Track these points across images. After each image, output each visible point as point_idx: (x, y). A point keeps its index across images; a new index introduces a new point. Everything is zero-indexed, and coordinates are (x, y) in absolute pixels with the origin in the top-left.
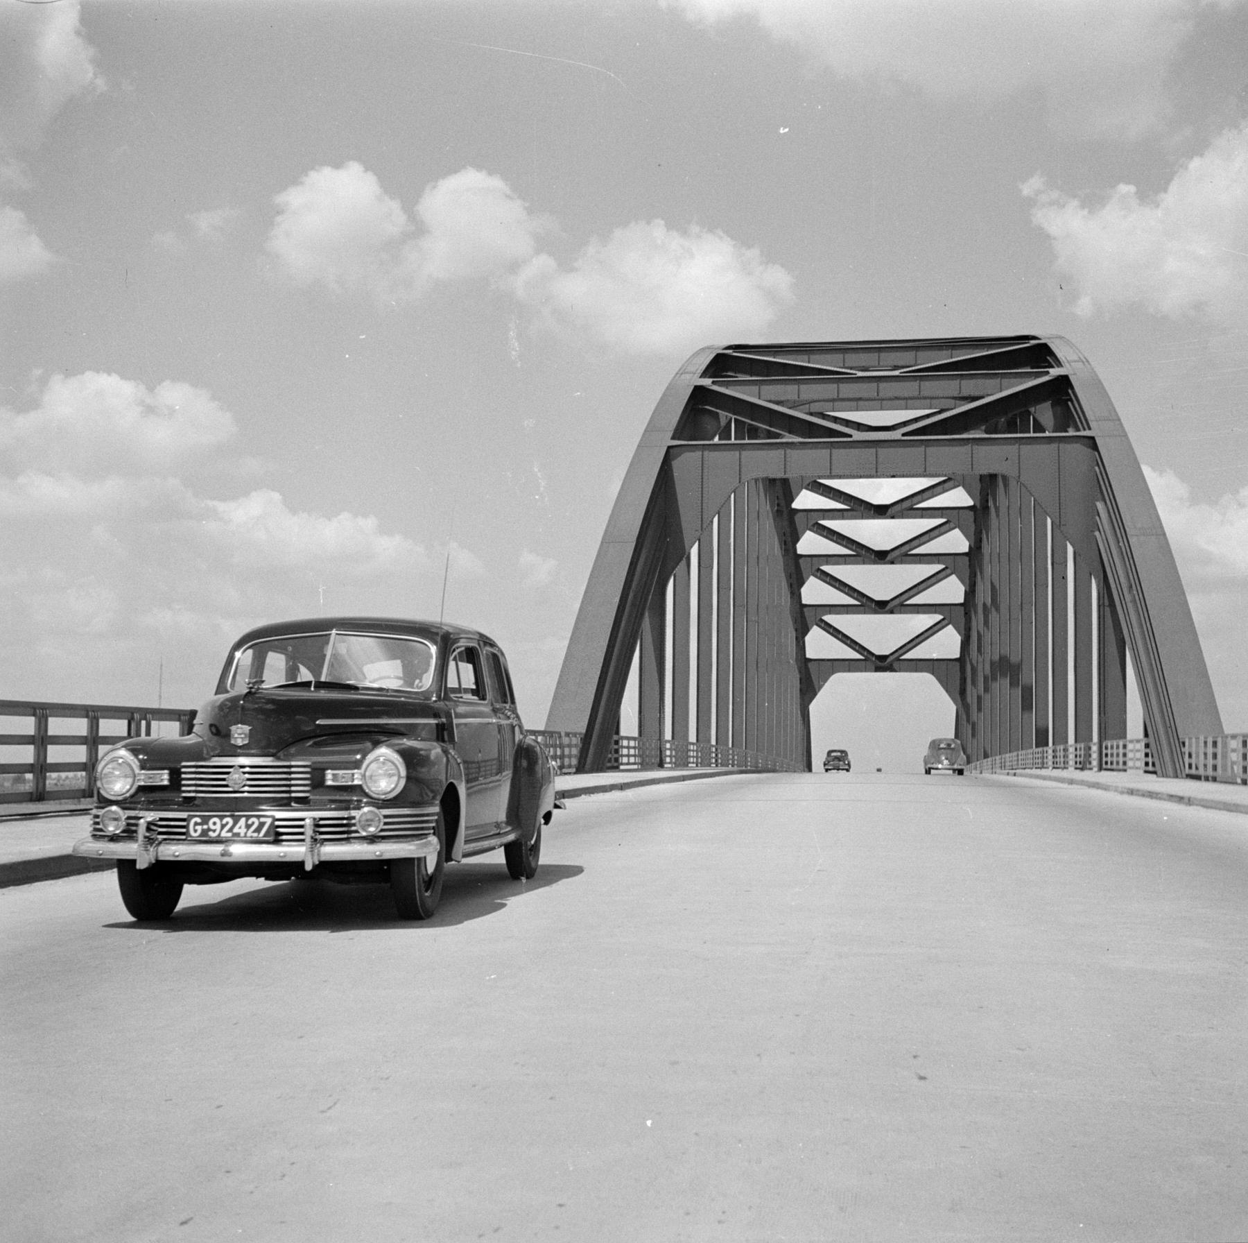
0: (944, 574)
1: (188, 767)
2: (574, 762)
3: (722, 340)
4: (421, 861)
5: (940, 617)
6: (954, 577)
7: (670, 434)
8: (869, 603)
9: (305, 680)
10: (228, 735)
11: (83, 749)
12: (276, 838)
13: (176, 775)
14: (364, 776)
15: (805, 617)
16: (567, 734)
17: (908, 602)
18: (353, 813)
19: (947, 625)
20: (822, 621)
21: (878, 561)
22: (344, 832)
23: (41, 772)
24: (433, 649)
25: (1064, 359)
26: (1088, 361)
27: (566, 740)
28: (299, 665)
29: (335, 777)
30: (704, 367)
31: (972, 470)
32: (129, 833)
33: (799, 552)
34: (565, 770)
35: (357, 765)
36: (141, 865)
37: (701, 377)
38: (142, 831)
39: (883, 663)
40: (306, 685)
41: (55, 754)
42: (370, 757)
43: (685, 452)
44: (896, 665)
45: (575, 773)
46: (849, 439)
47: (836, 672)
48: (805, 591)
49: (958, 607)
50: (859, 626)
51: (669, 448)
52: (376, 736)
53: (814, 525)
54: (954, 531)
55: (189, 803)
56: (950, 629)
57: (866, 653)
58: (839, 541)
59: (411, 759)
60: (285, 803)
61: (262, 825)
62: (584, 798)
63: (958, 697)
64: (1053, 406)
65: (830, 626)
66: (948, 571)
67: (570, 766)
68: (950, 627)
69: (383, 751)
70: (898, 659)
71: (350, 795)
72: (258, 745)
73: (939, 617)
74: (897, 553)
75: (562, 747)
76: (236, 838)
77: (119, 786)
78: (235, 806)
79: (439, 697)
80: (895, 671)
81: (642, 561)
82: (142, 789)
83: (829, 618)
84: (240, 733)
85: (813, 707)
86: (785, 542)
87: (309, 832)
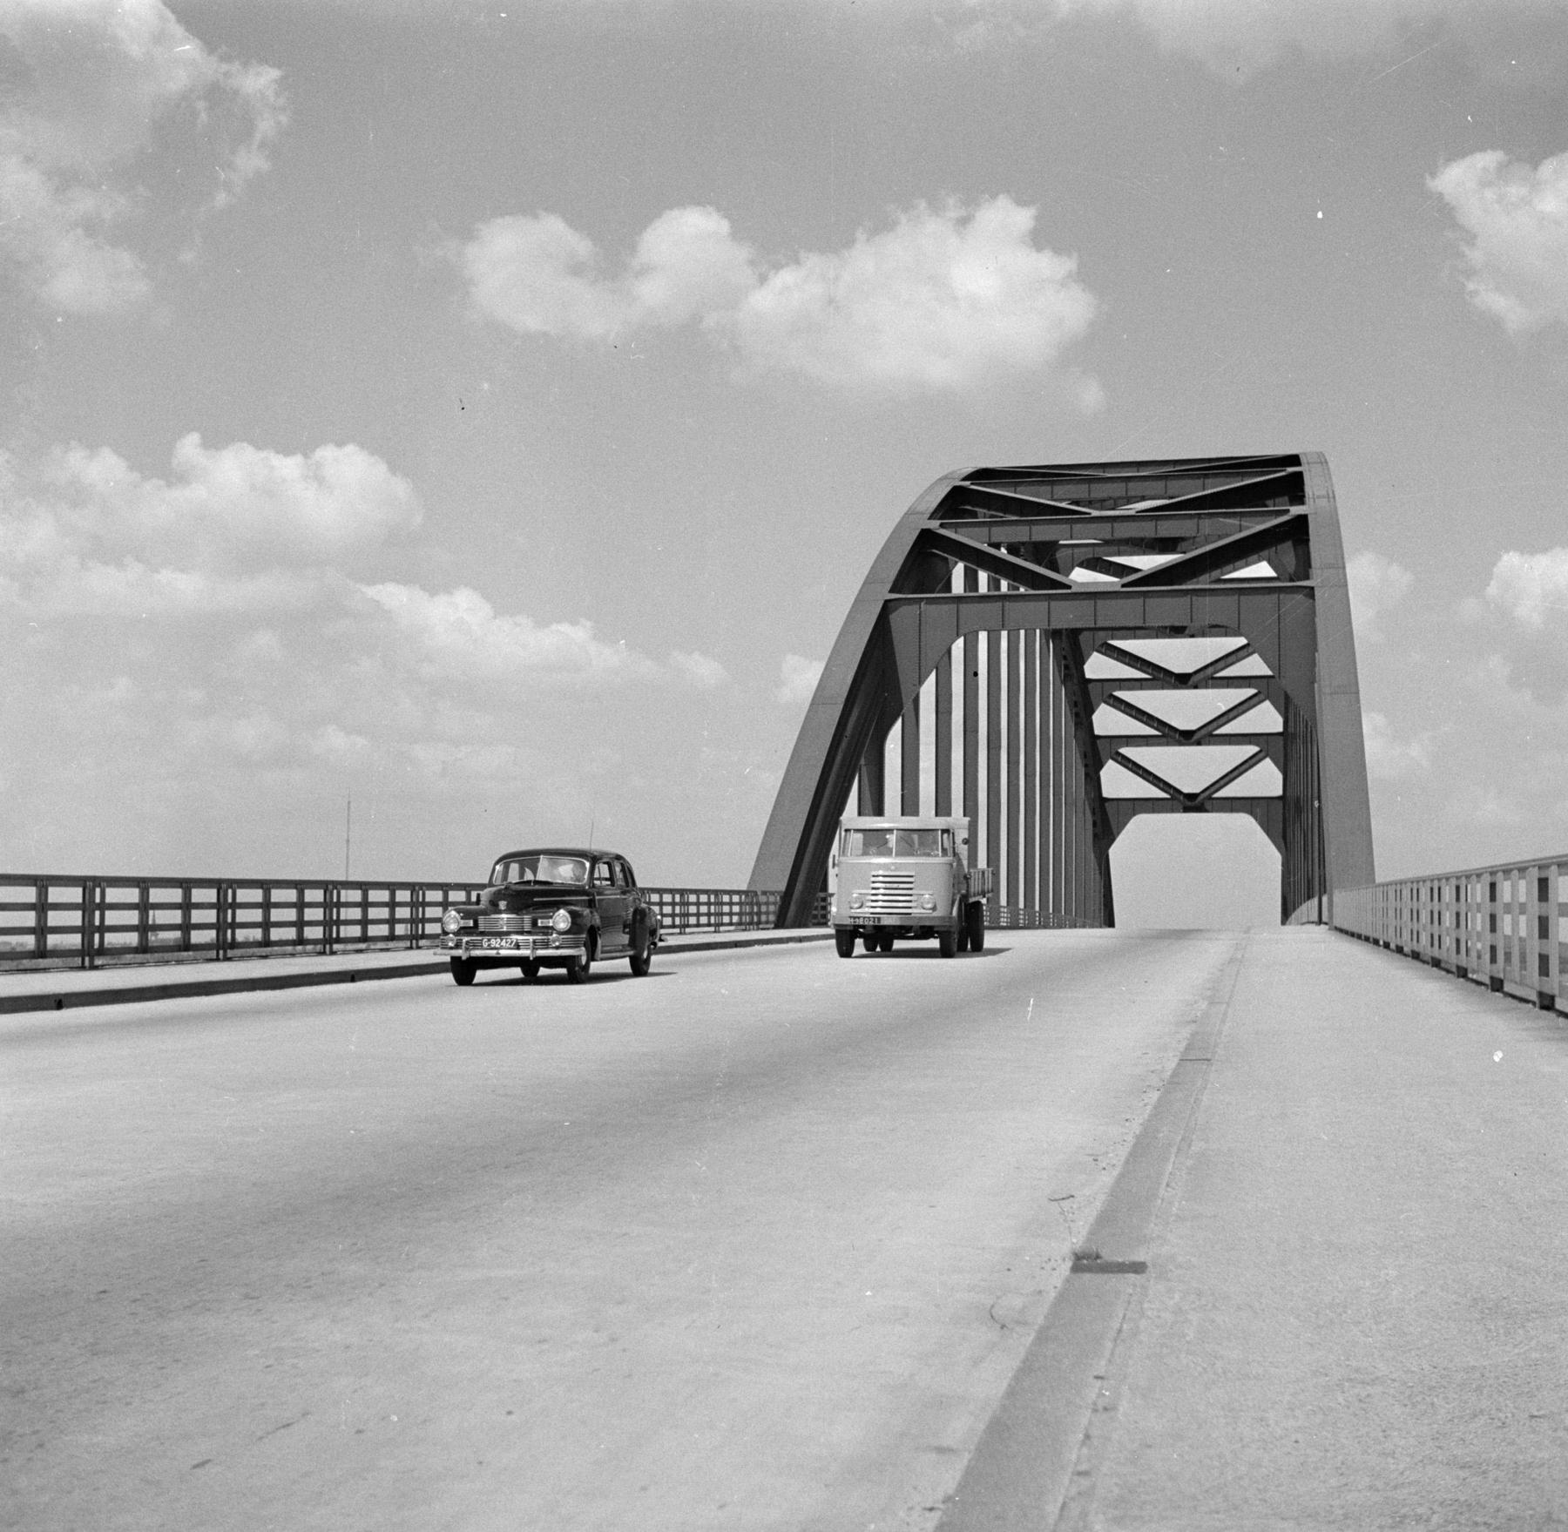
1: (481, 919)
2: (772, 918)
4: (579, 957)
6: (1267, 704)
7: (889, 586)
8: (1172, 733)
9: (529, 879)
10: (497, 905)
13: (476, 922)
14: (554, 922)
15: (1095, 751)
16: (764, 893)
17: (1218, 732)
18: (550, 937)
20: (1119, 754)
21: (1179, 685)
22: (546, 945)
23: (42, 933)
24: (588, 865)
25: (1311, 493)
26: (1334, 497)
27: (763, 899)
28: (527, 870)
29: (542, 923)
31: (1191, 622)
32: (458, 946)
33: (1088, 675)
34: (761, 926)
35: (551, 917)
36: (464, 958)
37: (929, 519)
38: (464, 945)
42: (557, 914)
43: (900, 606)
44: (1208, 805)
45: (774, 928)
46: (1069, 591)
47: (1141, 812)
48: (1097, 718)
49: (1277, 737)
50: (1163, 760)
51: (887, 602)
52: (557, 905)
53: (1102, 645)
54: (1251, 658)
55: (482, 934)
57: (1172, 792)
58: (1132, 663)
59: (574, 915)
60: (521, 933)
61: (512, 942)
62: (757, 947)
64: (1295, 546)
66: (1262, 697)
67: (767, 922)
68: (1268, 760)
69: (562, 912)
70: (1210, 798)
71: (548, 930)
72: (509, 910)
74: (1201, 675)
75: (759, 905)
76: (501, 948)
77: (453, 927)
78: (500, 934)
79: (590, 887)
82: (462, 928)
84: (503, 905)
85: (1114, 852)
86: (1066, 667)
87: (531, 944)
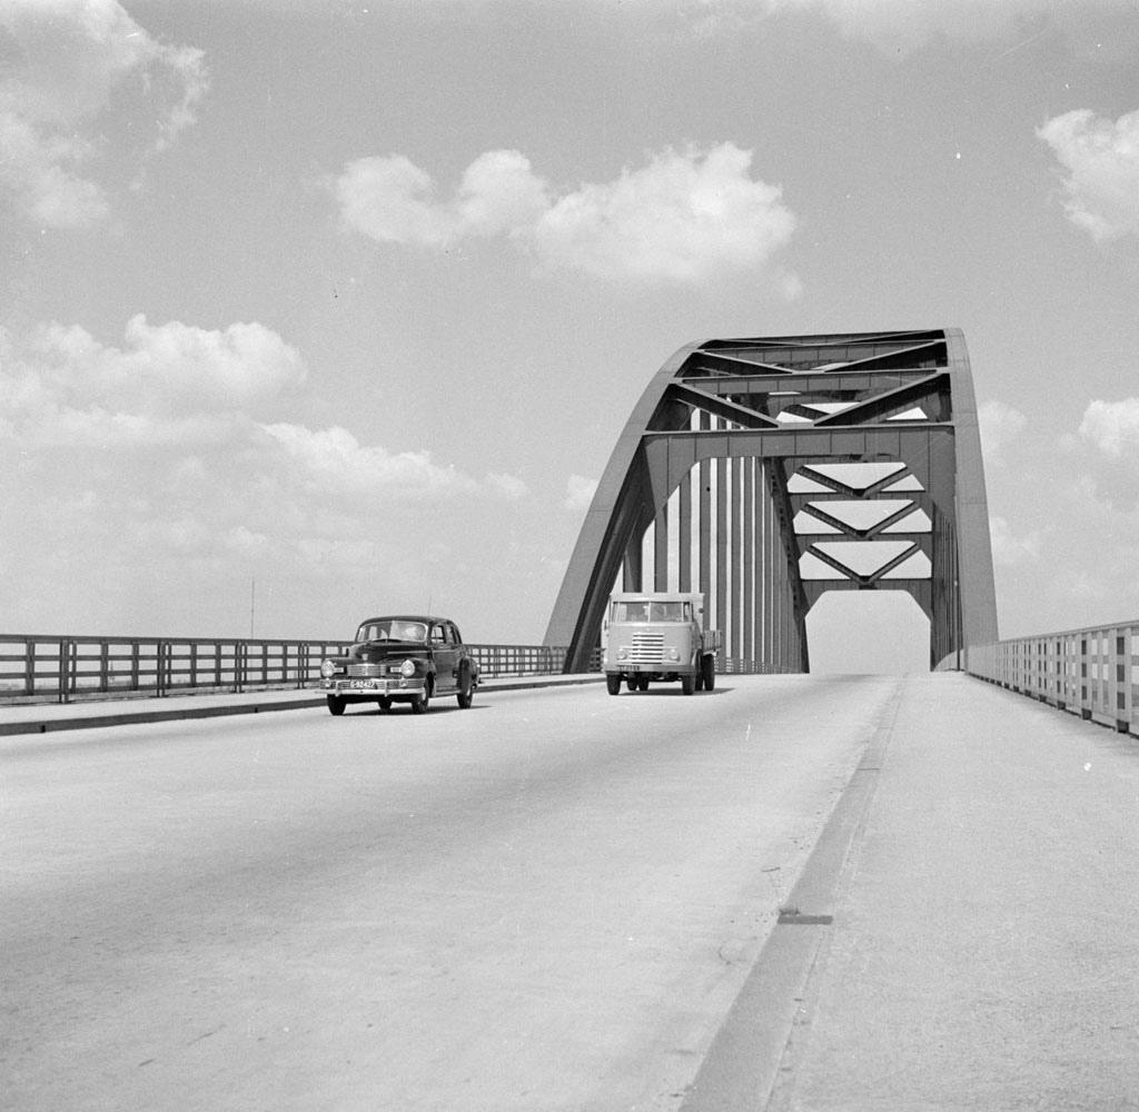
0: (912, 508)
1: (349, 667)
2: (561, 666)
3: (694, 337)
4: (420, 695)
5: (912, 544)
11: (130, 662)
12: (376, 687)
16: (555, 648)
19: (917, 550)
20: (812, 547)
22: (396, 686)
27: (554, 652)
30: (679, 366)
32: (332, 687)
35: (400, 666)
39: (866, 583)
40: (384, 640)
41: (39, 667)
44: (877, 584)
50: (842, 551)
51: (643, 437)
54: (908, 478)
55: (350, 678)
56: (920, 553)
59: (417, 664)
60: (379, 677)
62: (549, 688)
63: (931, 612)
64: (940, 395)
65: (820, 552)
66: (916, 506)
67: (557, 669)
68: (921, 553)
69: (408, 662)
70: (878, 579)
71: (397, 675)
73: (911, 544)
74: (872, 490)
75: (551, 656)
76: (364, 688)
77: (329, 673)
80: (876, 589)
81: (621, 518)
83: (818, 545)
84: (365, 657)
86: (774, 484)
